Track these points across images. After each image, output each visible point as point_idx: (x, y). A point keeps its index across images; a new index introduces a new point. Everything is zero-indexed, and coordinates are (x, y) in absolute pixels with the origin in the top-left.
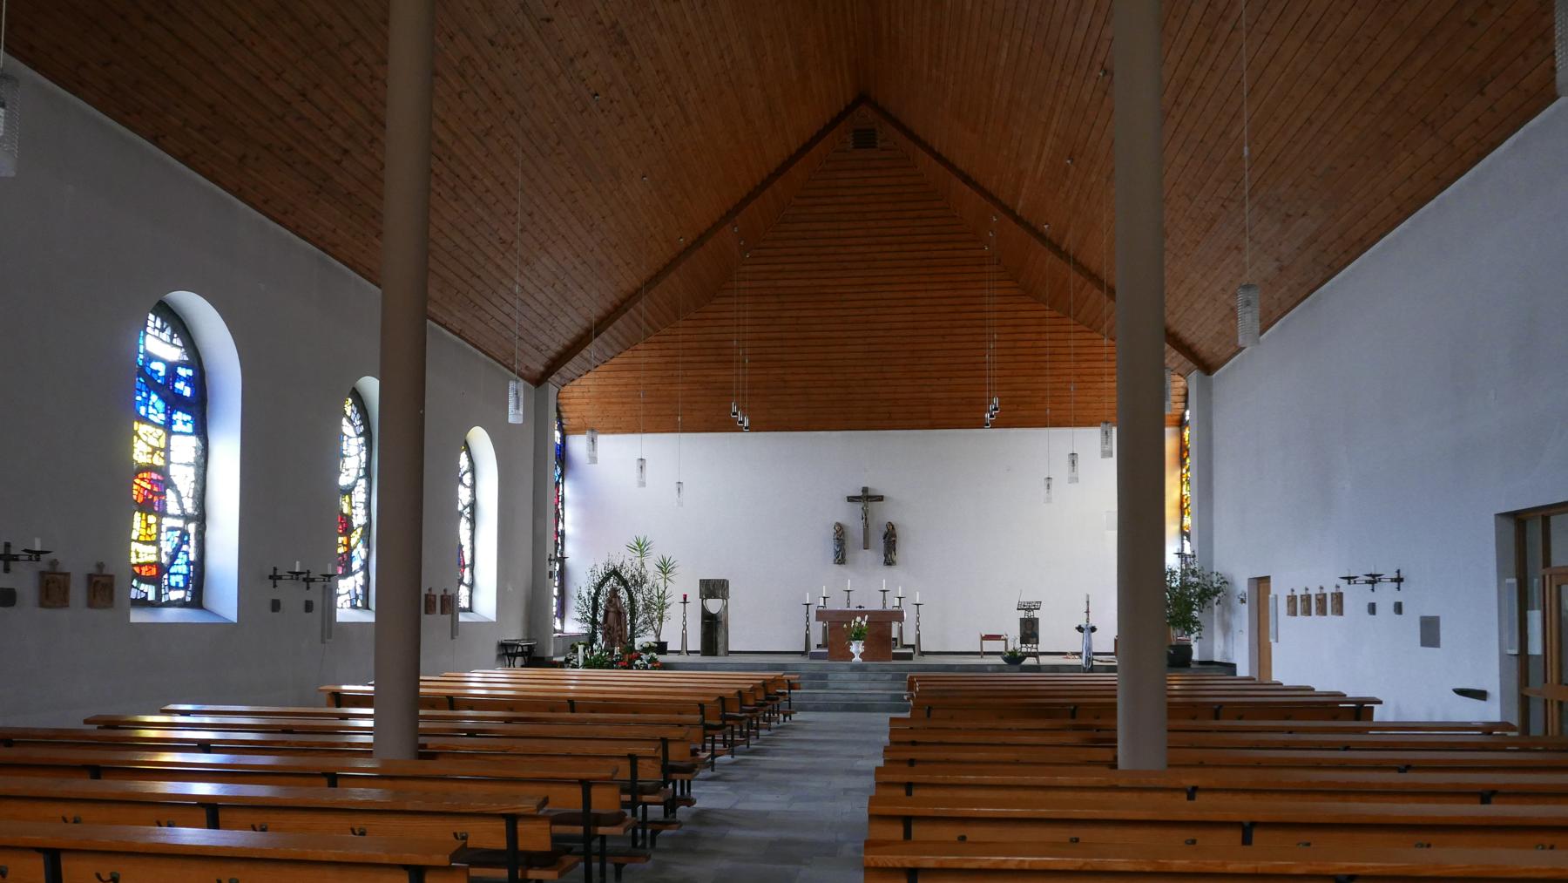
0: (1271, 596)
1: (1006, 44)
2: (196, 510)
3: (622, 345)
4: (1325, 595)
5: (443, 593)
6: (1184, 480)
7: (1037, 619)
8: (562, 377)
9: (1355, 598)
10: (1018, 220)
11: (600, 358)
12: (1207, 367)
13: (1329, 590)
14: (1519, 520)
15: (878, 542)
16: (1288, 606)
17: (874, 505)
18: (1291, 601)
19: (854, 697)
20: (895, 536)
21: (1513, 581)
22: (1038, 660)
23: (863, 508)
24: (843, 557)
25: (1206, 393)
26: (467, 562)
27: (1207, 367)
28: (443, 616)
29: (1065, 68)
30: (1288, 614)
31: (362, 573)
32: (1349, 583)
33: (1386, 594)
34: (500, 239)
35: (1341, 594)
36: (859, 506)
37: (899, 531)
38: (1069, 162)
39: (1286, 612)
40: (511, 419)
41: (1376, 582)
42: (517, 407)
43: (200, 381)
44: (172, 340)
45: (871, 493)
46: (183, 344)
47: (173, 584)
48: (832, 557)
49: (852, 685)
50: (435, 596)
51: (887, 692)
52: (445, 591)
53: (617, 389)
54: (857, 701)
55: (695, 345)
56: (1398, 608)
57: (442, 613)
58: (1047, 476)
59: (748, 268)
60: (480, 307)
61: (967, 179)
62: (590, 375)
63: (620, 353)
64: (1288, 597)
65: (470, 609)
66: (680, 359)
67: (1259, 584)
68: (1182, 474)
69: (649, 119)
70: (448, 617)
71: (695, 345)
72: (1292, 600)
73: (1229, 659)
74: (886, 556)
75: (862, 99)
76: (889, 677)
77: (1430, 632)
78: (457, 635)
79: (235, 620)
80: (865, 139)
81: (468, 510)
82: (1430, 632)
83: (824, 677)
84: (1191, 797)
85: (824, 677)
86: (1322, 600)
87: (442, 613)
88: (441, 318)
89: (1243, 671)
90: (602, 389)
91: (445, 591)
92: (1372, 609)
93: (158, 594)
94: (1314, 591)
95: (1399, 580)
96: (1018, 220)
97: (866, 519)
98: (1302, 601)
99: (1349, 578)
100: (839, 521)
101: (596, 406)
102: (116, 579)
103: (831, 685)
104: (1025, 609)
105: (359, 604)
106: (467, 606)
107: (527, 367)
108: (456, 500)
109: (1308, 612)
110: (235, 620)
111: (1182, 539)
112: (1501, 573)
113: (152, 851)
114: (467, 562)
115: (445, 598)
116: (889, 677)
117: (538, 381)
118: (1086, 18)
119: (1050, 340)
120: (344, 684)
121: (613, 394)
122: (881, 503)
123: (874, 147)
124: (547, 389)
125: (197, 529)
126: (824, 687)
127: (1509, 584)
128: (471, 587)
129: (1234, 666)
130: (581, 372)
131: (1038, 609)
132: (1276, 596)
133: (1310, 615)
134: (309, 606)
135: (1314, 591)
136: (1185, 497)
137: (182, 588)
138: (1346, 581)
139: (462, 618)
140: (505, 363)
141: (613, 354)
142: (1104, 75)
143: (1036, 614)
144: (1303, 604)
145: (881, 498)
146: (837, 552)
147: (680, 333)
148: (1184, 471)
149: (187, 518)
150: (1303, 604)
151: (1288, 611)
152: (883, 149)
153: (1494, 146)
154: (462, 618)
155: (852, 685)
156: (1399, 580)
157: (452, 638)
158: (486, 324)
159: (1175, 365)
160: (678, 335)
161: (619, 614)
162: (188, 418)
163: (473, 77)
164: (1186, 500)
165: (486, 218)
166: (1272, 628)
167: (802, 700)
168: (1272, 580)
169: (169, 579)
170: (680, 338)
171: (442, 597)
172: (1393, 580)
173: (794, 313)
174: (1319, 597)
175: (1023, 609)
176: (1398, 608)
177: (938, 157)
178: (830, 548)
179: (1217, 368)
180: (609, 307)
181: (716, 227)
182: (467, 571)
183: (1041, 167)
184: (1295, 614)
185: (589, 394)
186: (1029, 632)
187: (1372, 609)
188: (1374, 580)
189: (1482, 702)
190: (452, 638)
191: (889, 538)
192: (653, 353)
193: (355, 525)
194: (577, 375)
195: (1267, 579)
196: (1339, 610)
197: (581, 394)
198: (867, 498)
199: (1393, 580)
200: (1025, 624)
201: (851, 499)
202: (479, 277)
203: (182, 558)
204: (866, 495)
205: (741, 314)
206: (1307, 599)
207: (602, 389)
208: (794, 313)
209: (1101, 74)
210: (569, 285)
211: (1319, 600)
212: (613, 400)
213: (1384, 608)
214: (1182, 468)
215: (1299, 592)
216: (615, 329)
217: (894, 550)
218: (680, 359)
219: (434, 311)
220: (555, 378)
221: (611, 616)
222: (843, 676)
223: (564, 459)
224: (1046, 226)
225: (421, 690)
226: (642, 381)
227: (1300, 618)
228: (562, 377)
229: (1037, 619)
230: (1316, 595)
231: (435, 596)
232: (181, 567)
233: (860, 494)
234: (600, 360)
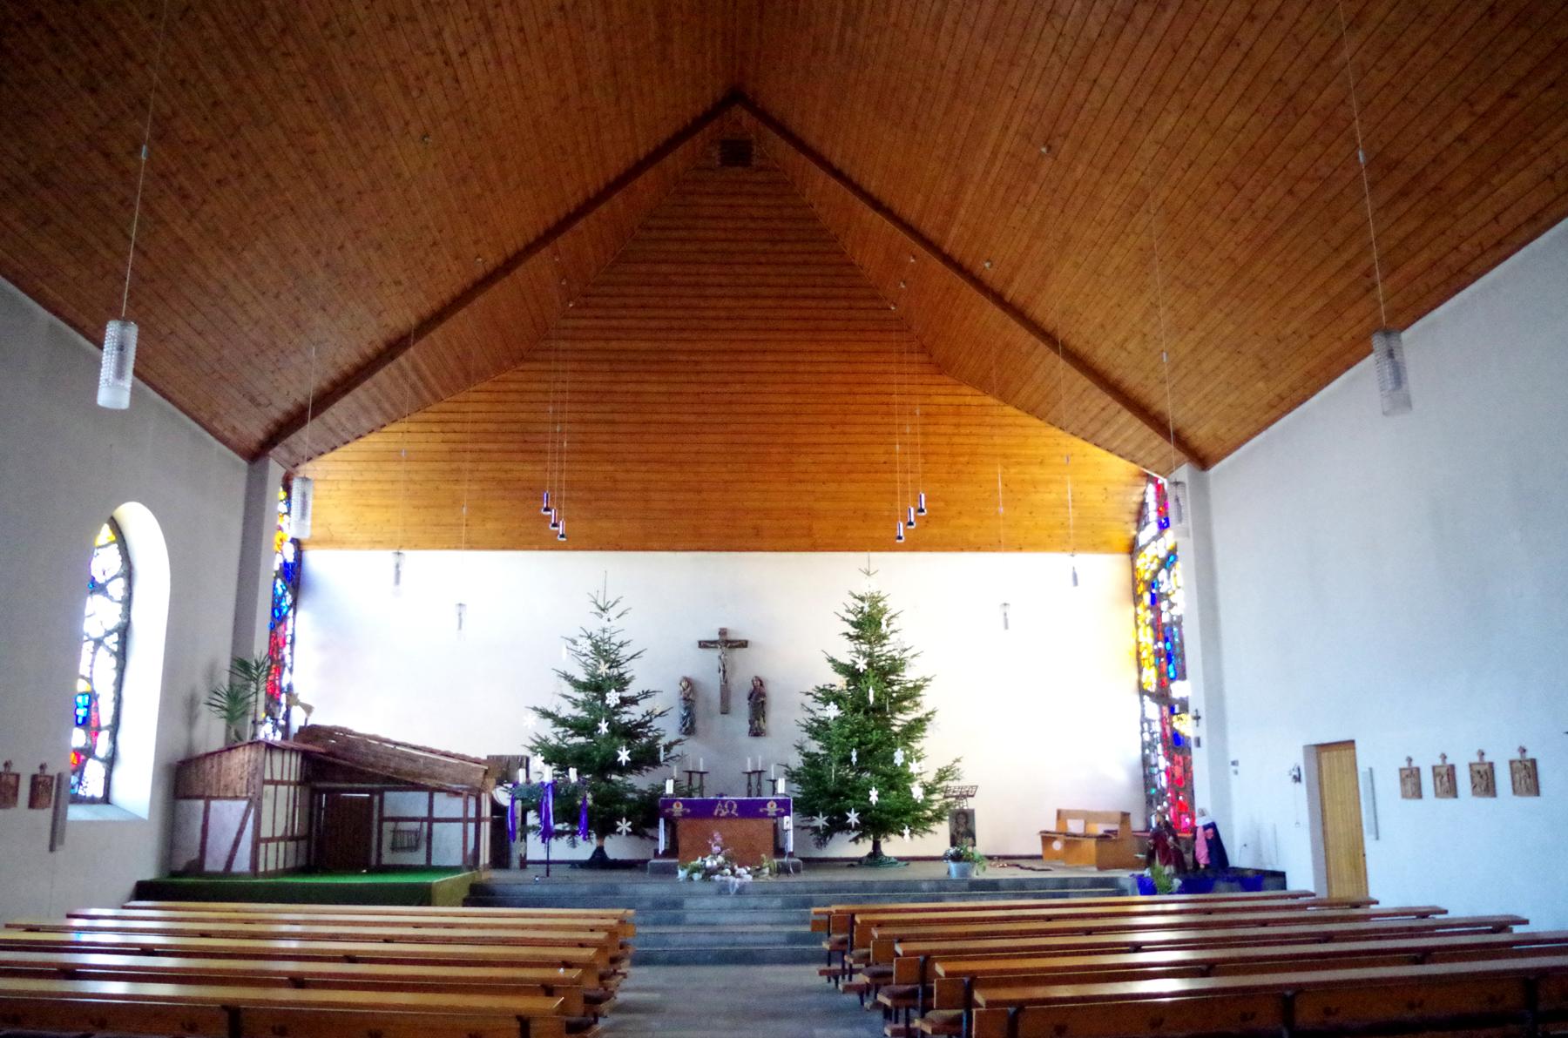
3: (384, 412)
5: (37, 771)
7: (972, 811)
8: (292, 452)
10: (947, 260)
11: (352, 430)
12: (1202, 461)
15: (742, 707)
19: (730, 939)
20: (764, 695)
23: (720, 657)
24: (692, 723)
25: (1202, 491)
27: (1202, 461)
28: (33, 812)
35: (1534, 762)
36: (713, 655)
40: (104, 397)
42: (120, 374)
45: (731, 637)
49: (723, 918)
50: (18, 776)
51: (777, 929)
52: (42, 767)
54: (734, 944)
55: (491, 427)
59: (570, 323)
62: (329, 456)
63: (384, 426)
65: (106, 799)
66: (469, 446)
68: (1136, 615)
69: (438, 34)
70: (44, 816)
71: (491, 427)
72: (1411, 780)
73: (1262, 864)
74: (751, 722)
75: (736, 96)
76: (777, 902)
78: (62, 842)
80: (737, 153)
81: (115, 637)
83: (677, 904)
85: (677, 904)
87: (32, 805)
89: (1302, 878)
91: (42, 767)
96: (947, 260)
97: (724, 672)
100: (688, 675)
103: (691, 917)
106: (99, 794)
107: (234, 429)
115: (40, 779)
116: (777, 902)
117: (256, 455)
122: (745, 649)
124: (265, 467)
126: (677, 921)
128: (111, 762)
129: (1282, 875)
130: (322, 447)
131: (972, 796)
139: (75, 813)
141: (371, 427)
143: (968, 804)
145: (744, 644)
146: (684, 718)
147: (471, 409)
154: (75, 813)
155: (723, 918)
157: (52, 848)
159: (1153, 460)
160: (473, 412)
167: (647, 945)
168: (1358, 745)
170: (470, 417)
171: (34, 777)
173: (632, 387)
174: (1482, 769)
177: (838, 174)
179: (1218, 459)
180: (369, 351)
181: (530, 249)
184: (1418, 794)
186: (962, 830)
190: (52, 848)
191: (757, 698)
192: (431, 437)
194: (315, 452)
197: (326, 493)
198: (728, 643)
201: (703, 645)
204: (724, 638)
205: (559, 386)
208: (632, 387)
214: (1136, 605)
216: (375, 385)
217: (763, 716)
218: (469, 446)
220: (279, 451)
222: (707, 903)
223: (298, 584)
228: (292, 452)
229: (972, 811)
233: (716, 637)
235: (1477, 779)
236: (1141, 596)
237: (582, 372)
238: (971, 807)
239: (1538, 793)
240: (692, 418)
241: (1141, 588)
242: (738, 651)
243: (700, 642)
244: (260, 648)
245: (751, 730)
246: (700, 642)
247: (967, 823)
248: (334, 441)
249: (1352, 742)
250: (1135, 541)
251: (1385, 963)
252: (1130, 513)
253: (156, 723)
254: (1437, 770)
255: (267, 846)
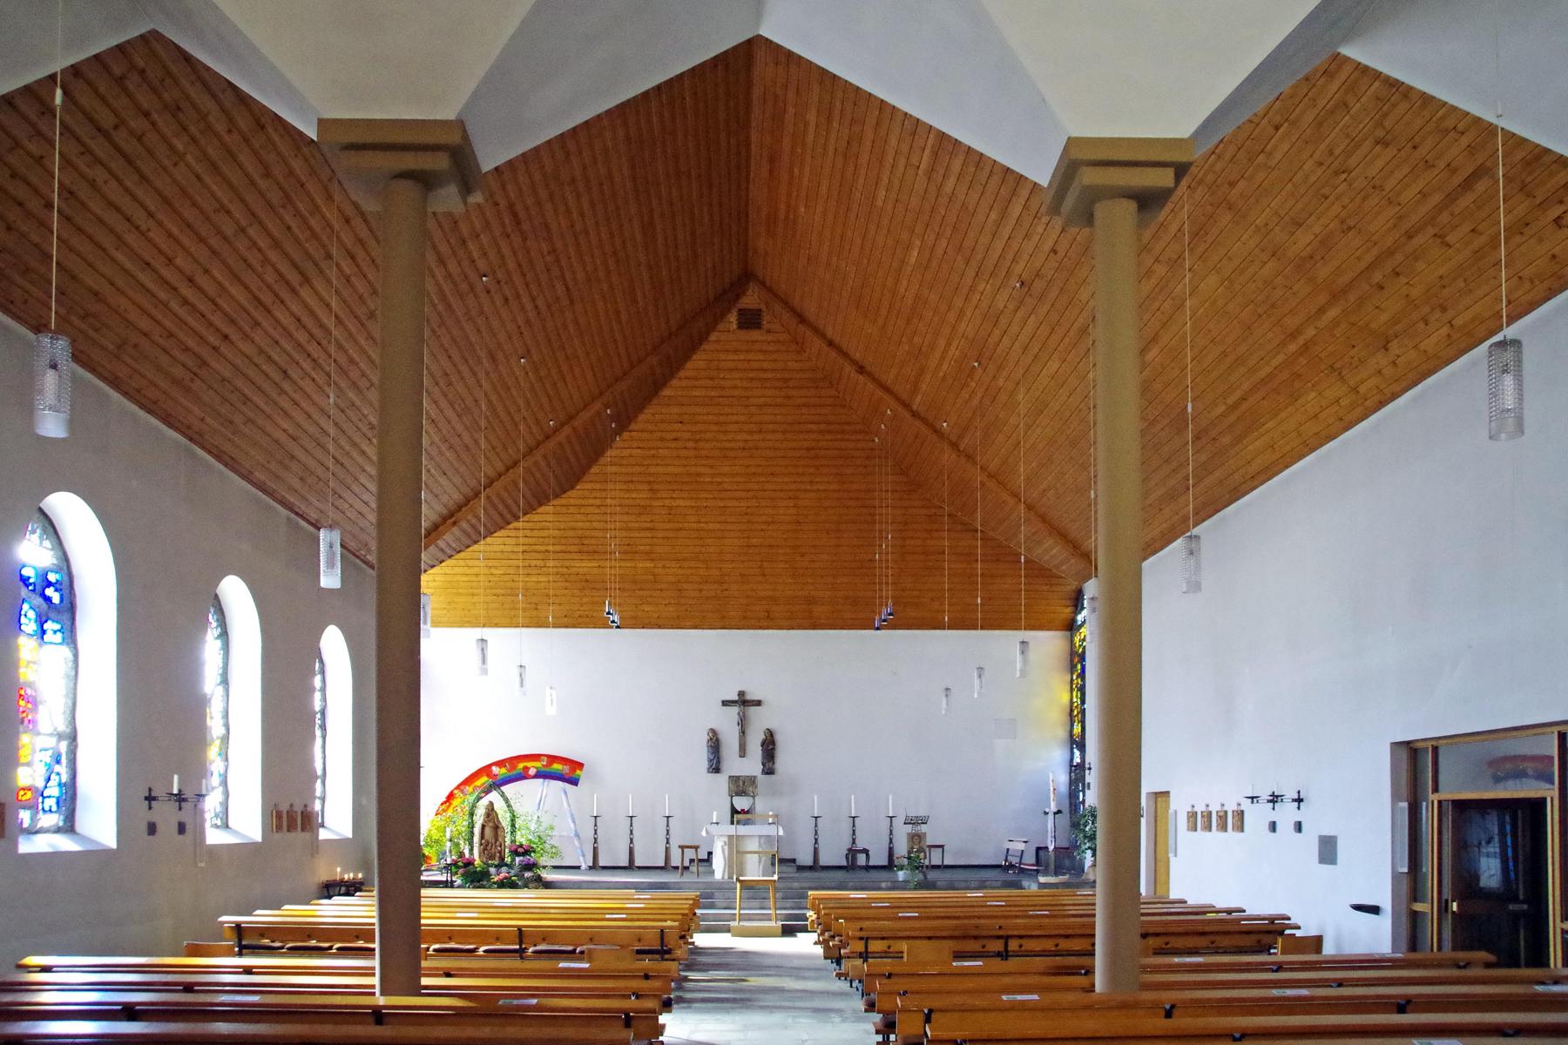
0: (1170, 811)
1: (918, 243)
2: (67, 727)
4: (1226, 812)
6: (1074, 686)
9: (1256, 817)
13: (1231, 807)
14: (1411, 748)
16: (1188, 822)
17: (752, 710)
18: (1192, 817)
21: (1405, 805)
22: (925, 876)
23: (739, 714)
26: (319, 772)
29: (980, 274)
30: (1188, 830)
31: (221, 789)
32: (1252, 802)
33: (1286, 814)
34: (370, 424)
36: (735, 710)
37: (778, 738)
38: (976, 364)
39: (1186, 828)
41: (1277, 802)
43: (68, 587)
44: (41, 543)
45: (748, 697)
46: (53, 546)
47: (47, 808)
48: (705, 764)
53: (466, 579)
56: (1299, 827)
57: (303, 830)
58: (945, 687)
60: (340, 497)
61: (861, 369)
62: (449, 562)
64: (1188, 813)
67: (1156, 798)
68: (1072, 680)
70: (307, 835)
72: (1192, 816)
77: (1328, 850)
79: (112, 843)
82: (1328, 850)
84: (1168, 1014)
86: (1223, 818)
88: (299, 508)
90: (449, 578)
92: (1273, 827)
93: (33, 819)
94: (1214, 808)
95: (1299, 800)
98: (1202, 816)
99: (1252, 798)
101: (442, 598)
102: (7, 807)
104: (914, 823)
105: (219, 823)
108: (312, 706)
109: (1208, 828)
110: (112, 843)
111: (1072, 749)
112: (1395, 797)
113: (1034, 1037)
114: (319, 772)
118: (1006, 232)
119: (686, 378)
120: (220, 916)
121: (462, 584)
123: (759, 328)
125: (69, 746)
127: (1402, 808)
132: (1176, 812)
133: (1226, 831)
134: (182, 828)
135: (1214, 808)
136: (1076, 704)
137: (55, 812)
138: (1250, 800)
140: (357, 554)
142: (1021, 287)
143: (923, 828)
144: (1202, 820)
145: (758, 703)
148: (1075, 677)
149: (60, 737)
150: (1202, 820)
151: (1188, 826)
152: (769, 331)
153: (1395, 396)
156: (1299, 800)
158: (344, 513)
161: (497, 828)
162: (58, 627)
163: (364, 260)
164: (1076, 707)
165: (358, 403)
166: (1171, 842)
169: (43, 802)
171: (302, 812)
172: (1294, 800)
174: (1222, 814)
175: (910, 823)
176: (1299, 827)
178: (702, 756)
182: (319, 781)
183: (945, 367)
185: (435, 584)
187: (1273, 827)
188: (1275, 799)
189: (1376, 916)
193: (215, 737)
195: (1166, 794)
196: (1240, 827)
199: (1294, 800)
200: (912, 838)
201: (725, 703)
202: (342, 464)
203: (54, 780)
206: (1208, 816)
207: (449, 578)
209: (1018, 285)
210: (432, 471)
211: (1220, 817)
212: (461, 591)
213: (1286, 826)
215: (1200, 808)
219: (292, 500)
221: (488, 831)
224: (945, 424)
225: (423, 922)
226: (494, 571)
227: (1201, 834)
230: (1217, 812)
231: (296, 812)
232: (53, 790)
233: (736, 698)
234: (455, 550)
235: (1219, 821)
236: (1076, 667)
237: (628, 491)
238: (923, 831)
239: (1242, 831)
240: (717, 526)
241: (1076, 660)
242: (753, 708)
243: (723, 702)
244: (54, 969)
245: (763, 770)
246: (723, 702)
247: (920, 842)
248: (443, 557)
249: (1168, 792)
250: (1074, 620)
251: (1225, 964)
252: (1070, 599)
253: (260, 811)
254: (1220, 814)
255: (871, 953)
